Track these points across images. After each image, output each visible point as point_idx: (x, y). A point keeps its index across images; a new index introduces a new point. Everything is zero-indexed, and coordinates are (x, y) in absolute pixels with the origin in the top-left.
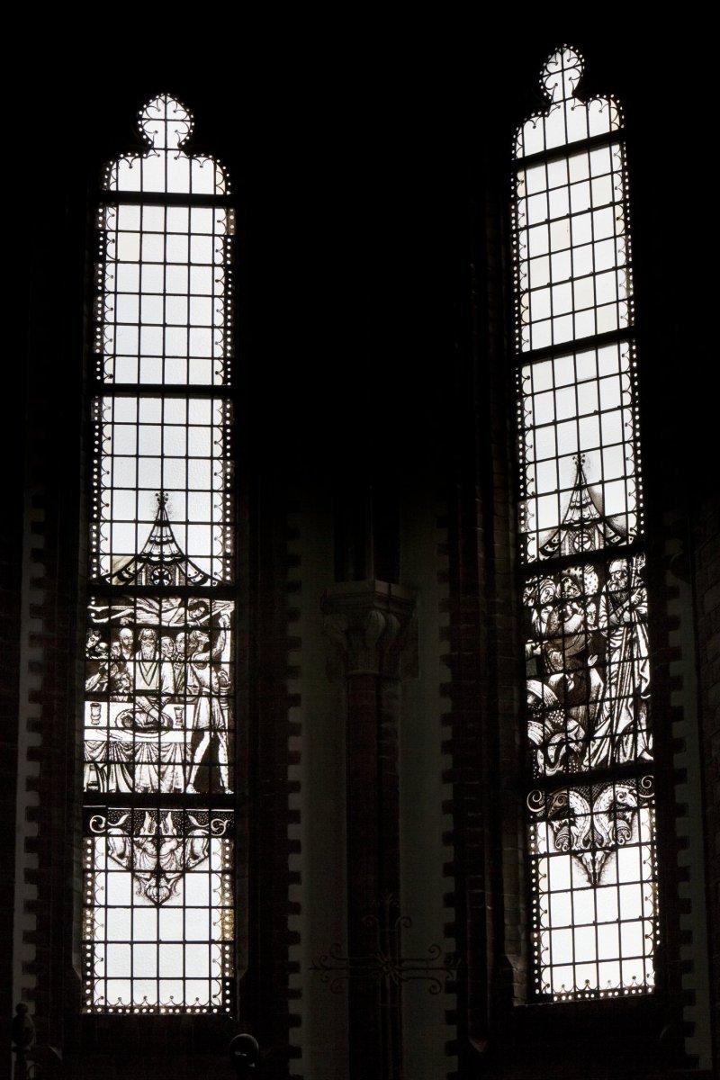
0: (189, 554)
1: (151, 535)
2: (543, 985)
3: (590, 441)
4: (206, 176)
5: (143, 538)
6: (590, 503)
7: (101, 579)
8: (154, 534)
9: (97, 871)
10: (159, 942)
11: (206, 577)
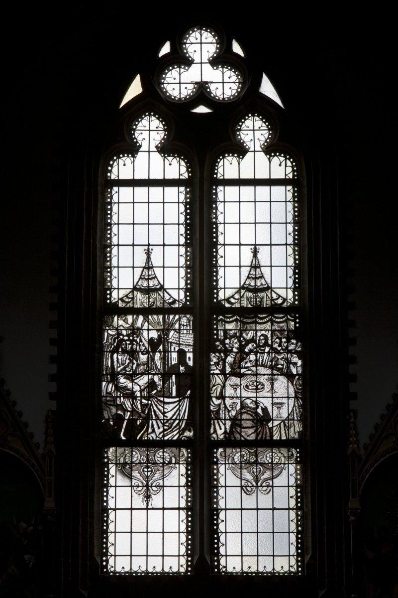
0: (273, 287)
1: (249, 274)
2: (109, 567)
3: (156, 239)
4: (281, 168)
5: (244, 278)
6: (154, 278)
7: (219, 302)
8: (143, 274)
9: (220, 509)
10: (164, 245)
11: (174, 301)
